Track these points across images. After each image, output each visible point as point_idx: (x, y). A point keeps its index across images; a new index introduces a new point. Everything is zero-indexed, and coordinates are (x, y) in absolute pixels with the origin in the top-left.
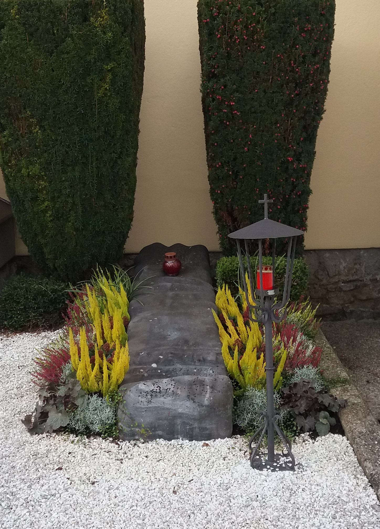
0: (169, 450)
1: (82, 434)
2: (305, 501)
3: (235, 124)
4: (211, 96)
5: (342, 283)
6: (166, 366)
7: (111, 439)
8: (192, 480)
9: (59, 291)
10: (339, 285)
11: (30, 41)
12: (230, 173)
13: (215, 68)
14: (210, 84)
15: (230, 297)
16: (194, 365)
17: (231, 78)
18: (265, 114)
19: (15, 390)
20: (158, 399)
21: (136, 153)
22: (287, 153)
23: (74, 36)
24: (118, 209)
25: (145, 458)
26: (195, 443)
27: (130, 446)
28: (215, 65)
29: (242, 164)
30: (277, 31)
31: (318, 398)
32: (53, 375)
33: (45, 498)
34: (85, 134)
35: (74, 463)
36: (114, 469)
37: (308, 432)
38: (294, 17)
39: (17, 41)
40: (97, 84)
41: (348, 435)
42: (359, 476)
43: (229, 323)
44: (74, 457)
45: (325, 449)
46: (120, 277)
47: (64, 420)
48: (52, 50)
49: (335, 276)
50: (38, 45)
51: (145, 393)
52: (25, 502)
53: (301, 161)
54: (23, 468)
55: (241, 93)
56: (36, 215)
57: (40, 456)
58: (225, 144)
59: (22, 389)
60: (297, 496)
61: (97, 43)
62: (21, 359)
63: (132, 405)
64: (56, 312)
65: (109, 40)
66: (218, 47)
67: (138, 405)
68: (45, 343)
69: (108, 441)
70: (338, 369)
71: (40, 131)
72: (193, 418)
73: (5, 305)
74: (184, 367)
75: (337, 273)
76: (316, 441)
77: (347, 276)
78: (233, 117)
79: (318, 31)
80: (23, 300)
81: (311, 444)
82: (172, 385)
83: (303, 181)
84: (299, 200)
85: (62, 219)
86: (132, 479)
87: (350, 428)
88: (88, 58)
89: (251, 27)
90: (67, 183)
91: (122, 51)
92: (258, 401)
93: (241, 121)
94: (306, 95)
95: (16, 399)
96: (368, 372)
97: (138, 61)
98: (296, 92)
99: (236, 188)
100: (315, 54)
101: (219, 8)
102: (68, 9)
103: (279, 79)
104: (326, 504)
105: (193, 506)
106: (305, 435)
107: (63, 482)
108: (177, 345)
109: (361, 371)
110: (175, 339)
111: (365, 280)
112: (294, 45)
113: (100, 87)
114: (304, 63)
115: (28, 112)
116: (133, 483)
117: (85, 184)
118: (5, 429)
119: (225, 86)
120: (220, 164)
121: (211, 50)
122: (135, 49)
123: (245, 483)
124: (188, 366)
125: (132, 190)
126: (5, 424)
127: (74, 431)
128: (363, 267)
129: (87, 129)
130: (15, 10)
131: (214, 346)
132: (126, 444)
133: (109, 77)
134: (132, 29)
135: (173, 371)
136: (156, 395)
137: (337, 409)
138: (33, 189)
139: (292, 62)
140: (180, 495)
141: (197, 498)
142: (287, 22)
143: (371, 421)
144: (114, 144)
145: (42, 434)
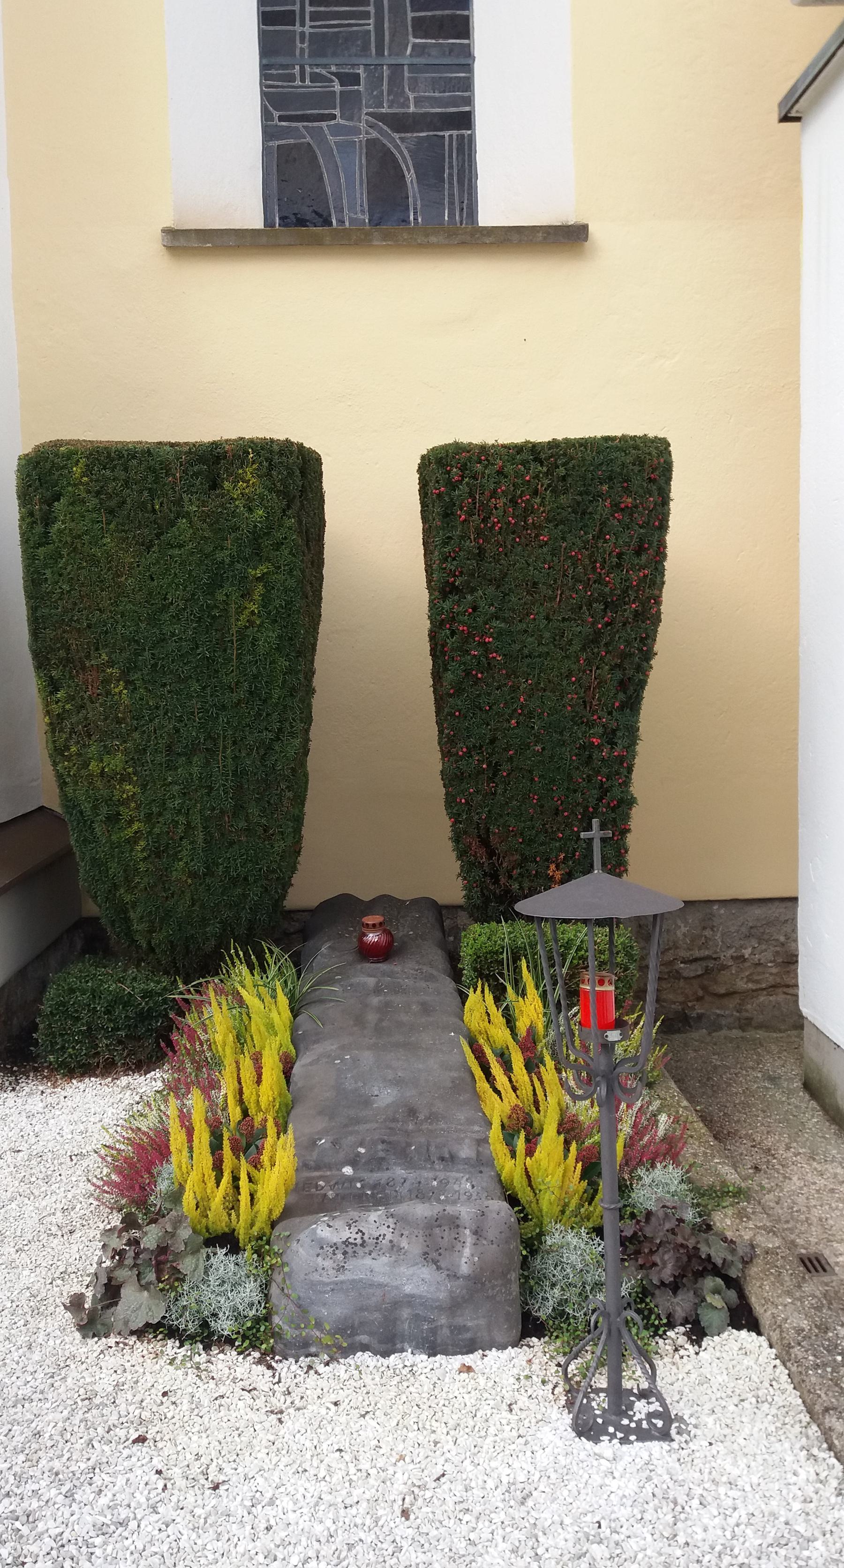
0: (383, 1381)
1: (192, 1338)
2: (711, 1536)
3: (493, 678)
4: (448, 626)
5: (681, 963)
6: (371, 1171)
7: (257, 1355)
8: (443, 1475)
9: (156, 993)
10: (676, 967)
11: (108, 524)
12: (484, 766)
13: (455, 576)
14: (447, 605)
15: (493, 1009)
16: (432, 1169)
17: (485, 594)
18: (549, 659)
19: (59, 1214)
20: (360, 1262)
21: (307, 731)
22: (590, 729)
23: (192, 515)
24: (272, 835)
25: (332, 1407)
26: (443, 1362)
27: (299, 1372)
28: (455, 571)
29: (506, 750)
30: (570, 510)
31: (699, 1246)
32: (137, 1188)
33: (103, 1534)
34: (211, 696)
35: (174, 1421)
36: (264, 1443)
37: (682, 1325)
38: (601, 484)
39: (84, 525)
40: (236, 603)
41: (768, 1334)
42: (815, 1451)
43: (497, 1070)
44: (174, 1403)
45: (725, 1372)
46: (275, 963)
47: (153, 1308)
48: (151, 541)
49: (670, 949)
50: (123, 531)
51: (331, 1247)
52: (54, 1545)
53: (616, 744)
54: (59, 1438)
55: (504, 620)
56: (116, 847)
57: (97, 1401)
58: (474, 714)
59: (72, 1213)
60: (689, 1523)
61: (235, 529)
62: (76, 1137)
63: (302, 1276)
64: (151, 1035)
65: (259, 522)
66: (462, 538)
67: (316, 1277)
68: (127, 1102)
69: (249, 1358)
70: (716, 1161)
71: (125, 691)
72: (436, 1308)
73: (50, 1025)
74: (412, 1176)
75: (671, 944)
76: (703, 1348)
77: (690, 950)
78: (489, 664)
79: (644, 509)
80: (86, 1014)
81: (693, 1356)
82: (388, 1227)
83: (620, 781)
84: (613, 815)
85: (165, 855)
86: (306, 1471)
87: (774, 1317)
88: (219, 556)
89: (523, 501)
90: (177, 787)
91: (282, 543)
92: (573, 1258)
93: (504, 672)
94: (624, 625)
95: (59, 1236)
96: (752, 1146)
97: (312, 563)
98: (606, 619)
99: (495, 794)
100: (639, 551)
101: (463, 468)
102: (181, 465)
103: (574, 596)
104: (760, 1545)
105: (450, 1558)
106: (677, 1334)
107: (147, 1484)
108: (395, 1120)
109: (737, 1144)
110: (388, 1106)
111: (722, 957)
112: (600, 535)
113: (240, 610)
114: (619, 568)
115: (104, 656)
116: (307, 1485)
117: (211, 788)
118: (29, 1319)
119: (475, 609)
120: (465, 750)
121: (447, 543)
122: (308, 541)
123: (566, 1482)
124: (418, 1172)
125: (300, 799)
126: (32, 1304)
127: (173, 1333)
128: (719, 935)
129: (216, 687)
130: (81, 468)
131: (470, 1122)
132: (289, 1368)
133: (259, 590)
134: (302, 505)
135: (388, 1184)
136: (355, 1252)
137: (738, 1271)
138: (110, 800)
139: (598, 565)
140: (419, 1521)
141: (458, 1530)
142: (587, 493)
143: (814, 1296)
144: (268, 715)
145: (107, 1336)
